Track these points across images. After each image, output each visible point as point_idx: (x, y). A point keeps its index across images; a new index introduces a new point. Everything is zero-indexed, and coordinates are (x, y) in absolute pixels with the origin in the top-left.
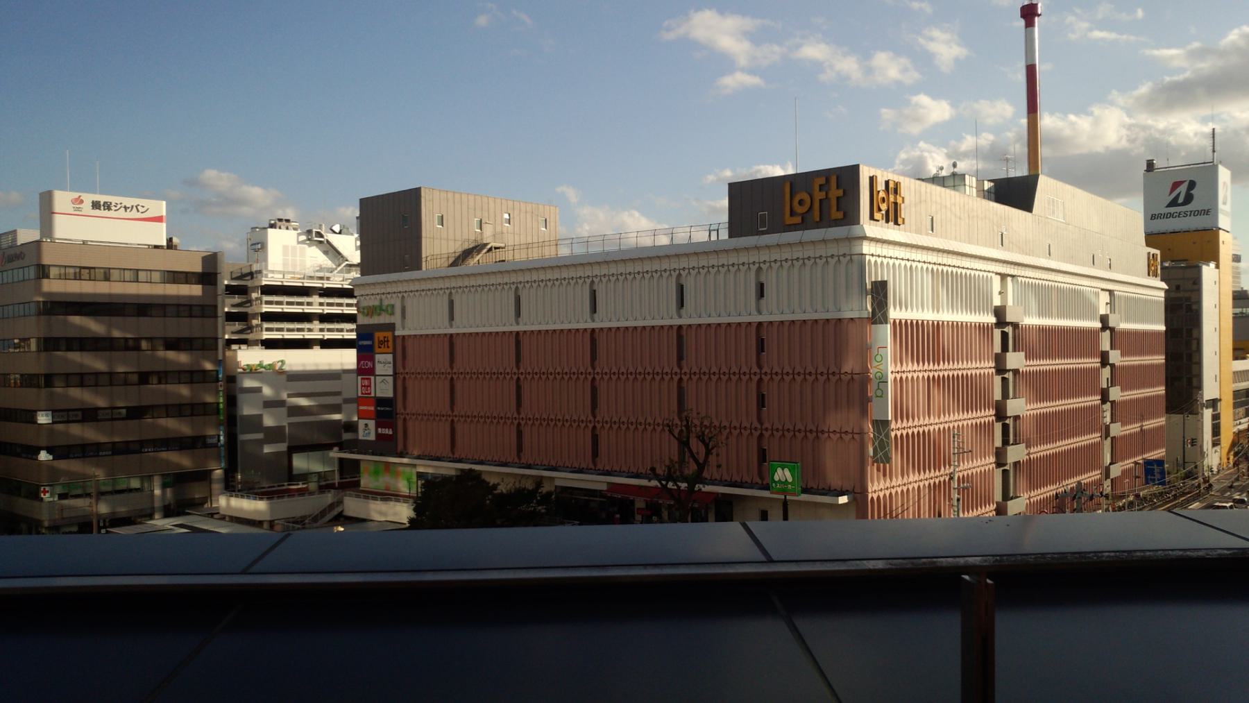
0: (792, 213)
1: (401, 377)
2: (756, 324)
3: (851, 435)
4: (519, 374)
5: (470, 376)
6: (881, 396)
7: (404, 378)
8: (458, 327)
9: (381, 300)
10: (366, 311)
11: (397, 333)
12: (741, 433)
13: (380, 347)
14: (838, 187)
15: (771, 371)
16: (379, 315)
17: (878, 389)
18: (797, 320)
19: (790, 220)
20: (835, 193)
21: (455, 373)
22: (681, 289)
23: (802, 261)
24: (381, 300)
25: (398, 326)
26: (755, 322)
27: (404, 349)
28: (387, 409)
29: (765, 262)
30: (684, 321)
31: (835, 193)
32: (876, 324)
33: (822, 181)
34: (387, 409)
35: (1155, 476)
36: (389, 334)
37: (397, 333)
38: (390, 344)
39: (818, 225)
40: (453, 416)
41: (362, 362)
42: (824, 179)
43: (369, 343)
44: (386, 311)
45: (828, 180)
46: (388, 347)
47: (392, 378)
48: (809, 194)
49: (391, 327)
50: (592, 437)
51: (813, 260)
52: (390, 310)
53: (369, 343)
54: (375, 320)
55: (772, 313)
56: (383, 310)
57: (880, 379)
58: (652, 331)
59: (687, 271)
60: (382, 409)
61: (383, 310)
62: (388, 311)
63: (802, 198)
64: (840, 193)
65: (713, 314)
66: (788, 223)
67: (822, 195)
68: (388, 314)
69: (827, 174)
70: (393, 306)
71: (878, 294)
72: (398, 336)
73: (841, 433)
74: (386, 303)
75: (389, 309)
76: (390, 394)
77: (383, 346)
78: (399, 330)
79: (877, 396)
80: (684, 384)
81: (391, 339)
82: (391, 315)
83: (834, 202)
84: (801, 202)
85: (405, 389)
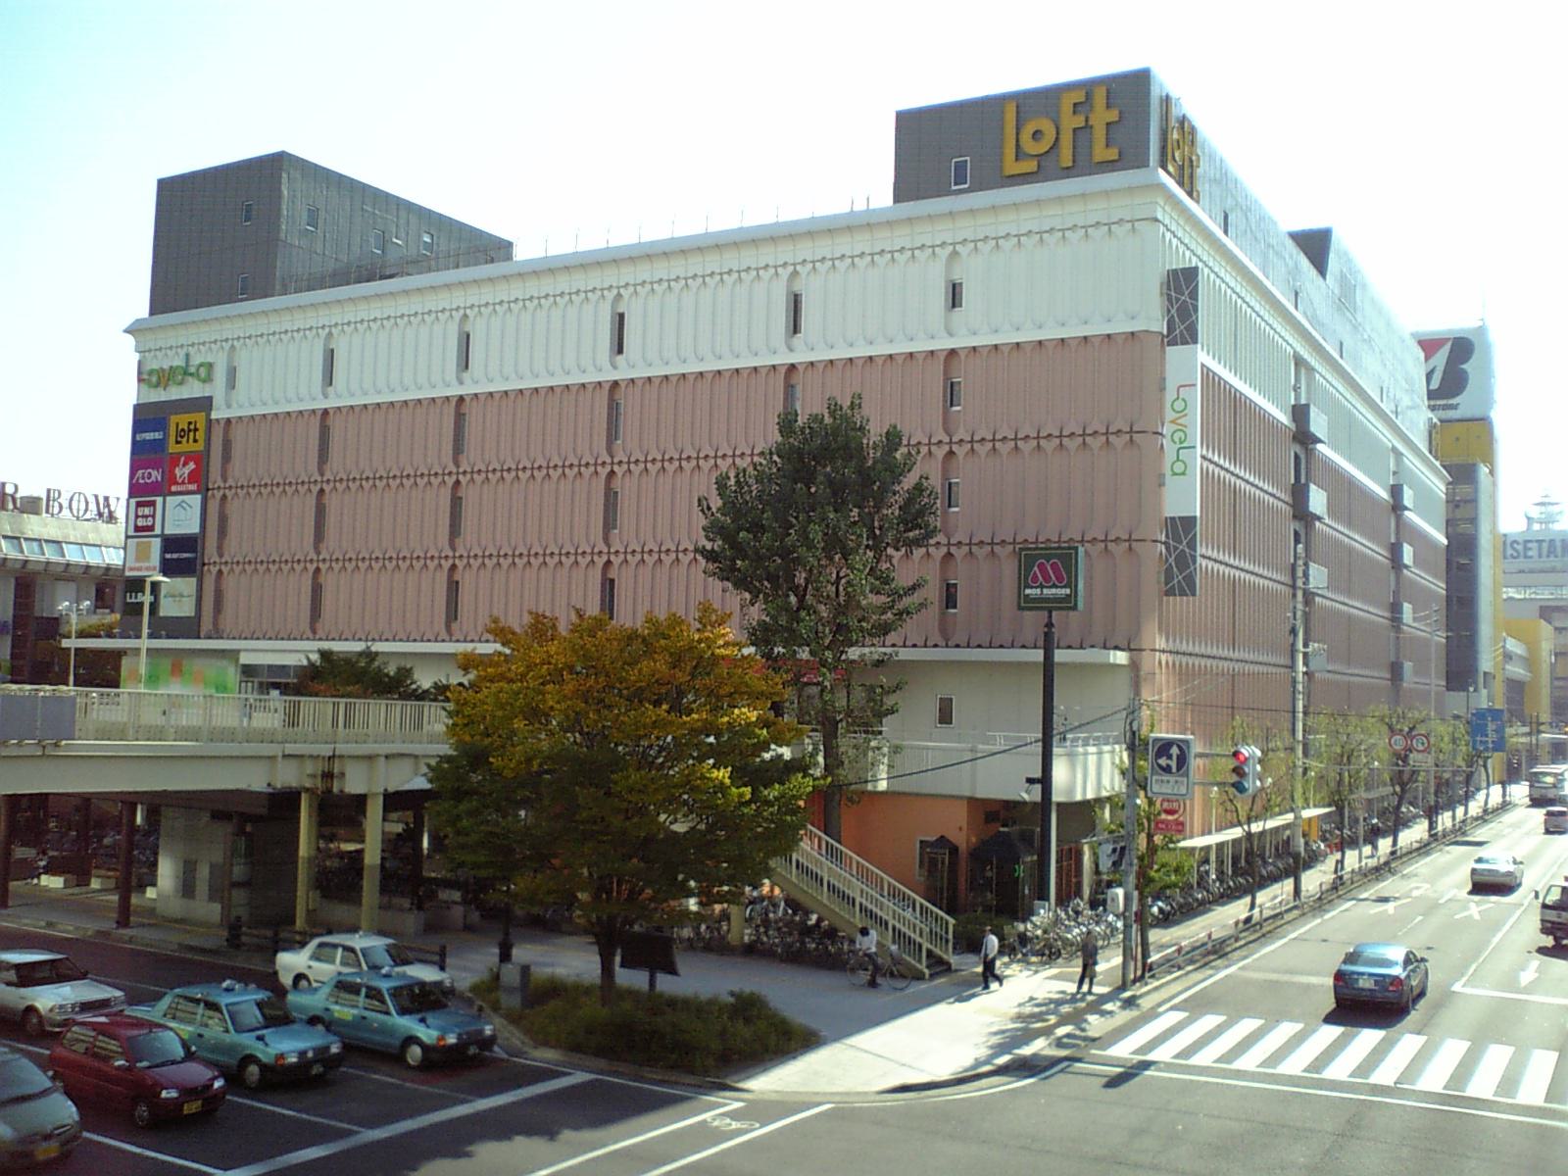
0: (1019, 155)
1: (219, 495)
2: (609, 384)
3: (967, 548)
4: (458, 473)
5: (257, 490)
6: (1183, 474)
7: (224, 497)
8: (241, 406)
9: (187, 355)
10: (154, 379)
11: (214, 416)
12: (627, 561)
13: (178, 442)
14: (1108, 106)
15: (994, 435)
16: (181, 383)
17: (1178, 459)
18: (983, 346)
19: (1012, 167)
20: (1101, 116)
21: (230, 487)
22: (465, 340)
23: (718, 277)
24: (187, 355)
25: (219, 401)
26: (841, 359)
27: (227, 445)
28: (185, 555)
29: (472, 306)
30: (798, 357)
31: (1101, 116)
32: (1176, 344)
33: (1080, 97)
34: (185, 555)
35: (1487, 736)
36: (200, 419)
37: (214, 416)
38: (200, 435)
39: (1068, 172)
40: (221, 563)
41: (140, 472)
42: (1083, 93)
43: (157, 435)
44: (196, 375)
45: (1089, 96)
46: (195, 441)
47: (168, 498)
48: (1053, 121)
49: (205, 404)
50: (603, 585)
51: (718, 277)
52: (207, 372)
53: (157, 435)
54: (175, 393)
55: (972, 330)
56: (191, 374)
57: (1181, 443)
58: (647, 385)
59: (631, 289)
60: (175, 556)
61: (191, 374)
62: (198, 375)
63: (1043, 128)
64: (1113, 115)
65: (591, 369)
66: (1007, 174)
67: (1079, 121)
68: (199, 380)
69: (1086, 92)
70: (210, 365)
71: (1179, 290)
72: (217, 420)
73: (992, 543)
74: (196, 360)
75: (203, 371)
76: (194, 528)
77: (185, 439)
78: (218, 409)
79: (1176, 474)
80: (617, 484)
81: (201, 425)
82: (204, 381)
83: (1100, 134)
84: (1037, 135)
85: (223, 520)
